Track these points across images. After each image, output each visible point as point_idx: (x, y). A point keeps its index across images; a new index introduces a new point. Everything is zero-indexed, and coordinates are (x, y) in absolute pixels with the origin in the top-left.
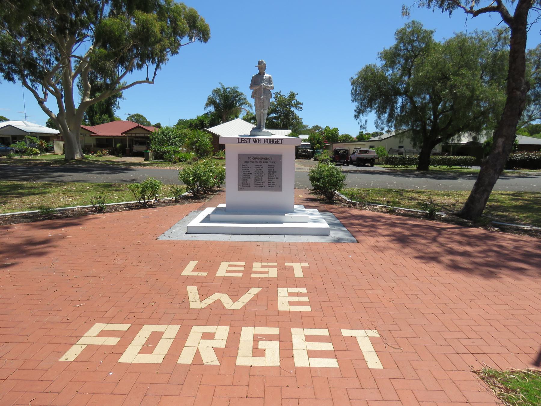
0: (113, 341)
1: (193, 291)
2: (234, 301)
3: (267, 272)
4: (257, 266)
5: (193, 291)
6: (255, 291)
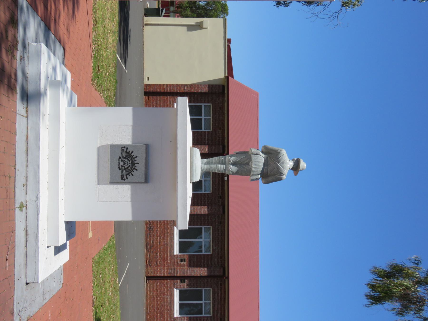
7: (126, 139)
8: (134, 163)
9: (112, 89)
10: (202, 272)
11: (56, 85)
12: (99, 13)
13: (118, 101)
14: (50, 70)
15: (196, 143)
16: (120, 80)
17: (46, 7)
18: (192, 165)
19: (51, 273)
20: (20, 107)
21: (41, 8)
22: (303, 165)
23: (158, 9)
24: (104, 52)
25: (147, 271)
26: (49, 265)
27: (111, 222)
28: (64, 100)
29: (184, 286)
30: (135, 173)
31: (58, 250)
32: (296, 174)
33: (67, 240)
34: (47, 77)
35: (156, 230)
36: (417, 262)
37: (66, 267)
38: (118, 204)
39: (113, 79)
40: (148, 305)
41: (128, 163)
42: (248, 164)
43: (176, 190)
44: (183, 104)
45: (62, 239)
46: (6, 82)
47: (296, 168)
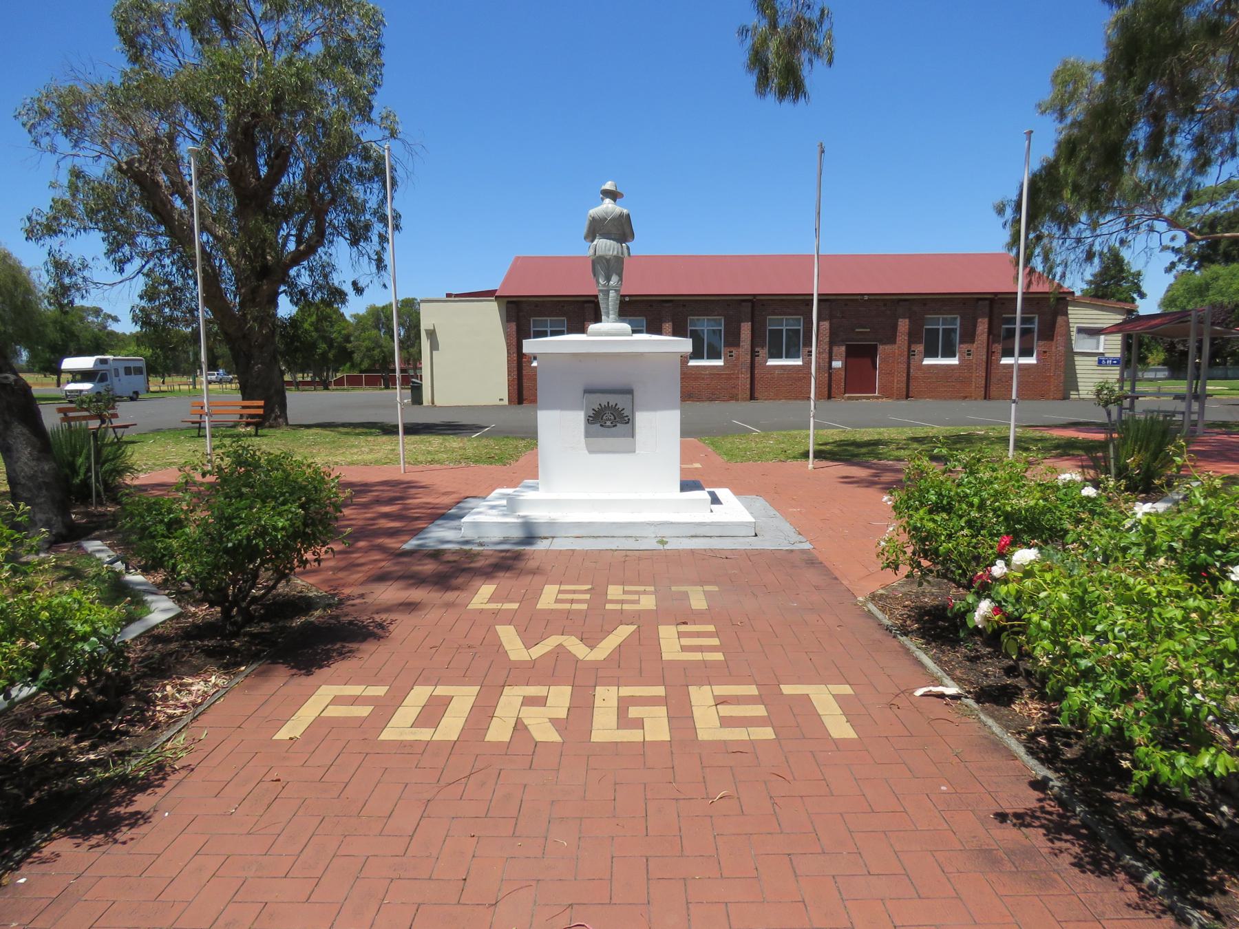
0: (364, 711)
1: (508, 636)
2: (592, 647)
3: (637, 602)
4: (614, 591)
5: (508, 636)
6: (624, 631)
7: (578, 418)
8: (608, 407)
9: (515, 442)
10: (746, 329)
11: (512, 504)
12: (421, 458)
13: (530, 435)
14: (494, 512)
15: (582, 330)
16: (502, 433)
17: (417, 519)
18: (610, 334)
19: (743, 508)
20: (541, 546)
21: (419, 524)
22: (609, 186)
23: (413, 388)
24: (470, 452)
25: (744, 399)
26: (733, 509)
27: (682, 443)
28: (530, 495)
29: (763, 352)
30: (620, 406)
31: (715, 500)
32: (622, 196)
33: (703, 489)
34: (504, 515)
35: (694, 389)
36: (744, 31)
37: (737, 492)
38: (659, 427)
39: (504, 437)
40: (786, 398)
41: (608, 415)
42: (608, 261)
43: (642, 354)
44: (530, 346)
45: (703, 495)
46: (510, 562)
47: (613, 195)
